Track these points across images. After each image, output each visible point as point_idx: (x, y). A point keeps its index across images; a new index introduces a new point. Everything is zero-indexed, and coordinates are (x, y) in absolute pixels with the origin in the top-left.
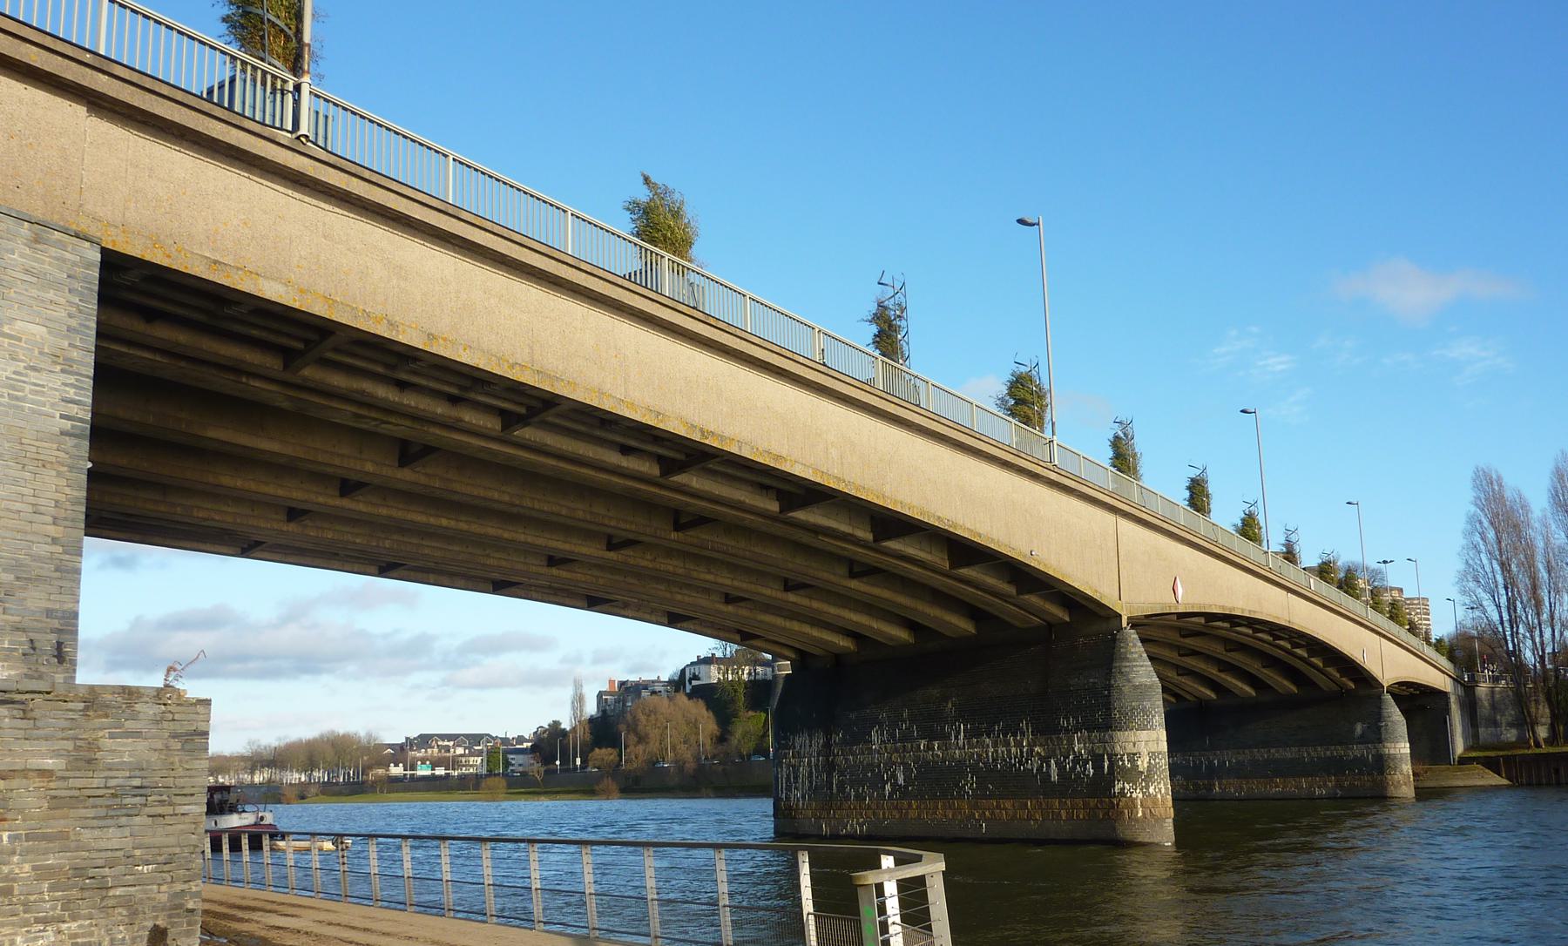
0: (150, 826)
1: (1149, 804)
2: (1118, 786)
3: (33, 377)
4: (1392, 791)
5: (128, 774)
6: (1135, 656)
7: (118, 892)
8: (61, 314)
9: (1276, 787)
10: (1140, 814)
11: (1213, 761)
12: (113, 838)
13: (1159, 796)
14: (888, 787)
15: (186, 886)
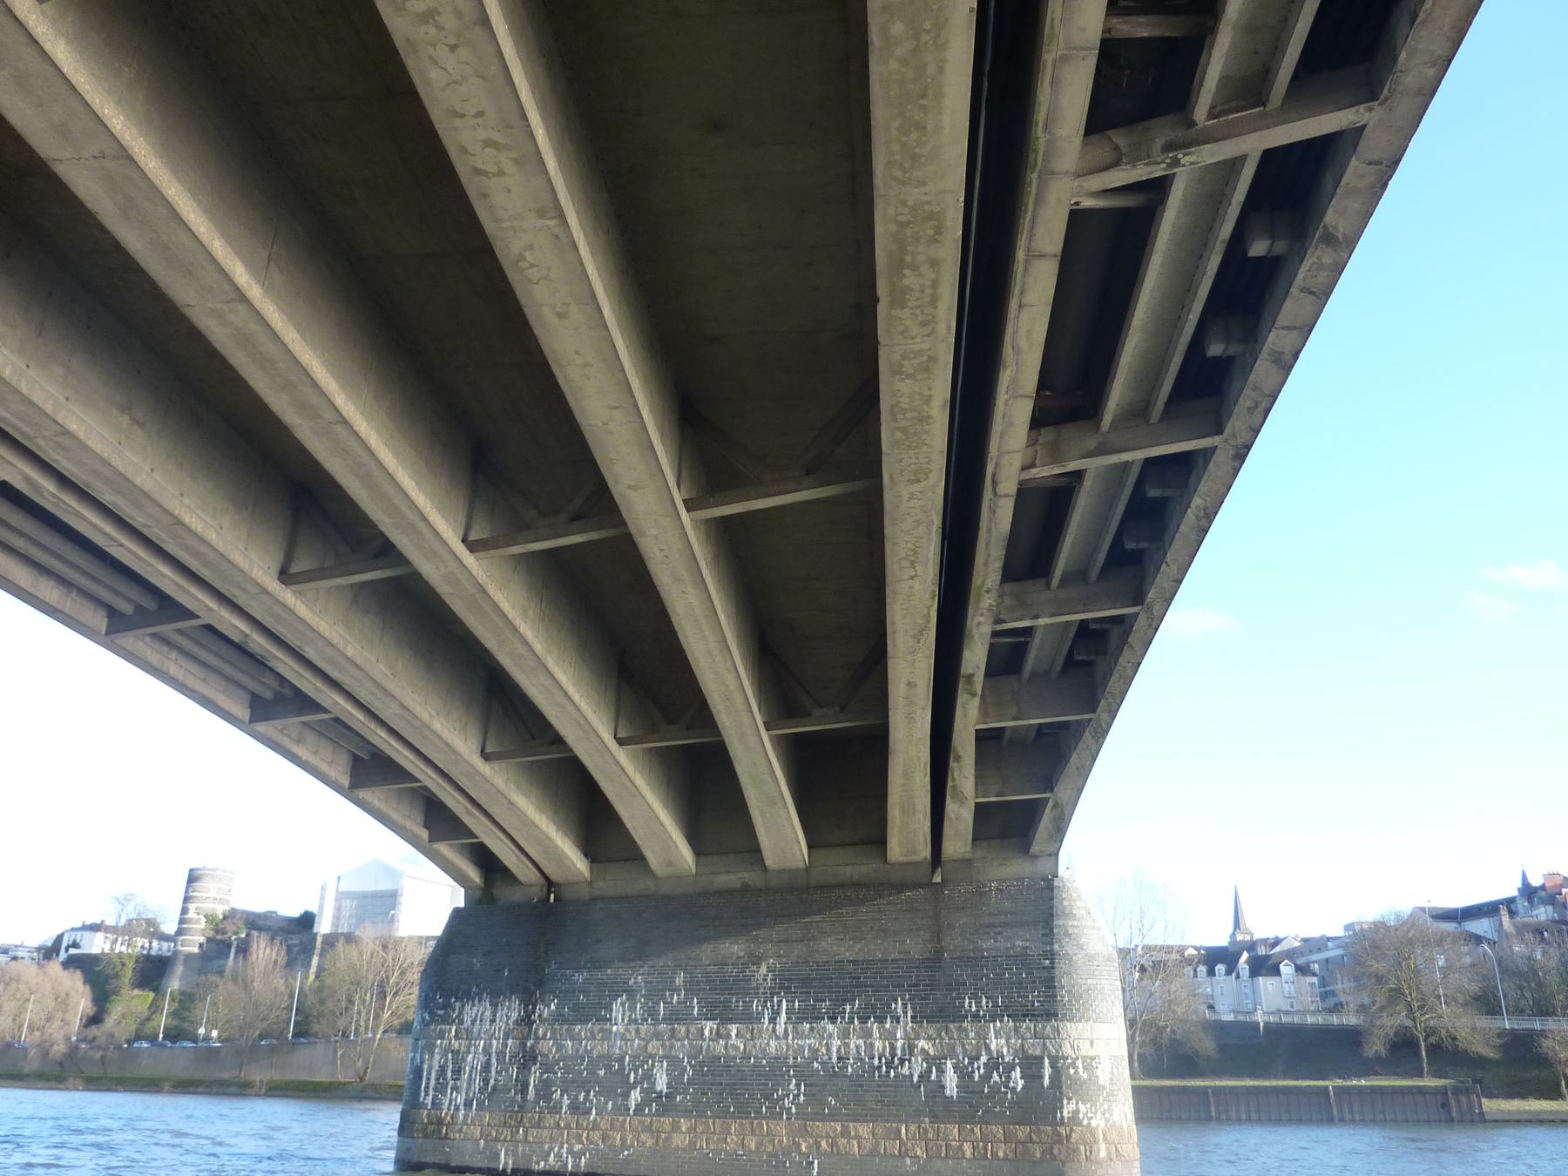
1: (1114, 1137)
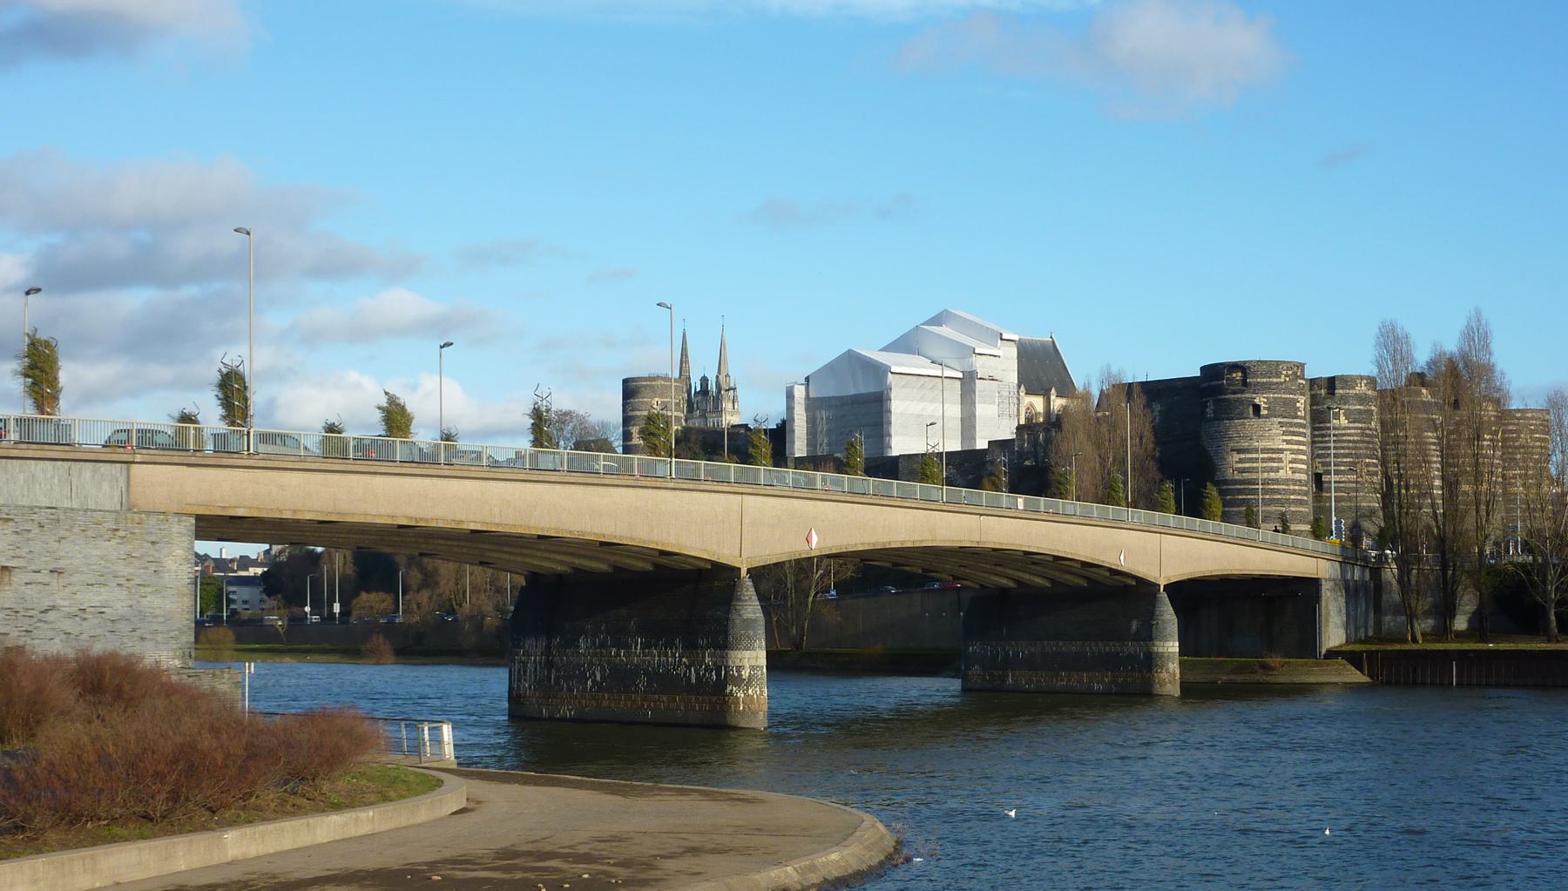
1: (748, 701)
2: (729, 688)
4: (1158, 689)
6: (747, 598)
8: (186, 544)
9: (1062, 680)
10: (741, 708)
11: (1008, 651)
13: (755, 696)
14: (589, 682)
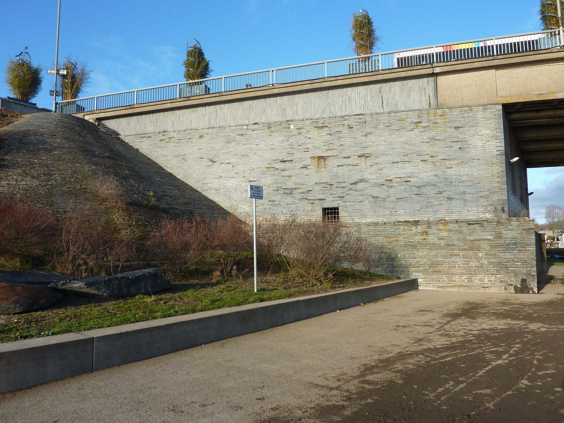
0: (519, 253)
3: (488, 143)
5: (511, 240)
7: (511, 269)
12: (508, 256)
15: (531, 269)
